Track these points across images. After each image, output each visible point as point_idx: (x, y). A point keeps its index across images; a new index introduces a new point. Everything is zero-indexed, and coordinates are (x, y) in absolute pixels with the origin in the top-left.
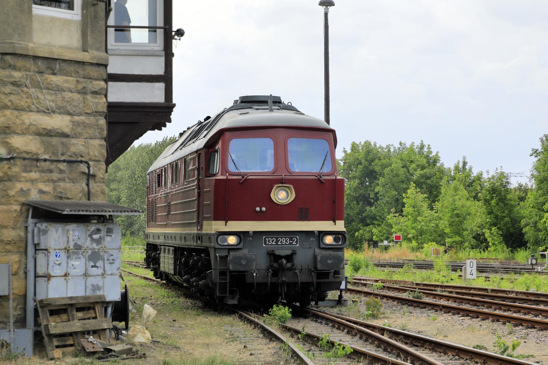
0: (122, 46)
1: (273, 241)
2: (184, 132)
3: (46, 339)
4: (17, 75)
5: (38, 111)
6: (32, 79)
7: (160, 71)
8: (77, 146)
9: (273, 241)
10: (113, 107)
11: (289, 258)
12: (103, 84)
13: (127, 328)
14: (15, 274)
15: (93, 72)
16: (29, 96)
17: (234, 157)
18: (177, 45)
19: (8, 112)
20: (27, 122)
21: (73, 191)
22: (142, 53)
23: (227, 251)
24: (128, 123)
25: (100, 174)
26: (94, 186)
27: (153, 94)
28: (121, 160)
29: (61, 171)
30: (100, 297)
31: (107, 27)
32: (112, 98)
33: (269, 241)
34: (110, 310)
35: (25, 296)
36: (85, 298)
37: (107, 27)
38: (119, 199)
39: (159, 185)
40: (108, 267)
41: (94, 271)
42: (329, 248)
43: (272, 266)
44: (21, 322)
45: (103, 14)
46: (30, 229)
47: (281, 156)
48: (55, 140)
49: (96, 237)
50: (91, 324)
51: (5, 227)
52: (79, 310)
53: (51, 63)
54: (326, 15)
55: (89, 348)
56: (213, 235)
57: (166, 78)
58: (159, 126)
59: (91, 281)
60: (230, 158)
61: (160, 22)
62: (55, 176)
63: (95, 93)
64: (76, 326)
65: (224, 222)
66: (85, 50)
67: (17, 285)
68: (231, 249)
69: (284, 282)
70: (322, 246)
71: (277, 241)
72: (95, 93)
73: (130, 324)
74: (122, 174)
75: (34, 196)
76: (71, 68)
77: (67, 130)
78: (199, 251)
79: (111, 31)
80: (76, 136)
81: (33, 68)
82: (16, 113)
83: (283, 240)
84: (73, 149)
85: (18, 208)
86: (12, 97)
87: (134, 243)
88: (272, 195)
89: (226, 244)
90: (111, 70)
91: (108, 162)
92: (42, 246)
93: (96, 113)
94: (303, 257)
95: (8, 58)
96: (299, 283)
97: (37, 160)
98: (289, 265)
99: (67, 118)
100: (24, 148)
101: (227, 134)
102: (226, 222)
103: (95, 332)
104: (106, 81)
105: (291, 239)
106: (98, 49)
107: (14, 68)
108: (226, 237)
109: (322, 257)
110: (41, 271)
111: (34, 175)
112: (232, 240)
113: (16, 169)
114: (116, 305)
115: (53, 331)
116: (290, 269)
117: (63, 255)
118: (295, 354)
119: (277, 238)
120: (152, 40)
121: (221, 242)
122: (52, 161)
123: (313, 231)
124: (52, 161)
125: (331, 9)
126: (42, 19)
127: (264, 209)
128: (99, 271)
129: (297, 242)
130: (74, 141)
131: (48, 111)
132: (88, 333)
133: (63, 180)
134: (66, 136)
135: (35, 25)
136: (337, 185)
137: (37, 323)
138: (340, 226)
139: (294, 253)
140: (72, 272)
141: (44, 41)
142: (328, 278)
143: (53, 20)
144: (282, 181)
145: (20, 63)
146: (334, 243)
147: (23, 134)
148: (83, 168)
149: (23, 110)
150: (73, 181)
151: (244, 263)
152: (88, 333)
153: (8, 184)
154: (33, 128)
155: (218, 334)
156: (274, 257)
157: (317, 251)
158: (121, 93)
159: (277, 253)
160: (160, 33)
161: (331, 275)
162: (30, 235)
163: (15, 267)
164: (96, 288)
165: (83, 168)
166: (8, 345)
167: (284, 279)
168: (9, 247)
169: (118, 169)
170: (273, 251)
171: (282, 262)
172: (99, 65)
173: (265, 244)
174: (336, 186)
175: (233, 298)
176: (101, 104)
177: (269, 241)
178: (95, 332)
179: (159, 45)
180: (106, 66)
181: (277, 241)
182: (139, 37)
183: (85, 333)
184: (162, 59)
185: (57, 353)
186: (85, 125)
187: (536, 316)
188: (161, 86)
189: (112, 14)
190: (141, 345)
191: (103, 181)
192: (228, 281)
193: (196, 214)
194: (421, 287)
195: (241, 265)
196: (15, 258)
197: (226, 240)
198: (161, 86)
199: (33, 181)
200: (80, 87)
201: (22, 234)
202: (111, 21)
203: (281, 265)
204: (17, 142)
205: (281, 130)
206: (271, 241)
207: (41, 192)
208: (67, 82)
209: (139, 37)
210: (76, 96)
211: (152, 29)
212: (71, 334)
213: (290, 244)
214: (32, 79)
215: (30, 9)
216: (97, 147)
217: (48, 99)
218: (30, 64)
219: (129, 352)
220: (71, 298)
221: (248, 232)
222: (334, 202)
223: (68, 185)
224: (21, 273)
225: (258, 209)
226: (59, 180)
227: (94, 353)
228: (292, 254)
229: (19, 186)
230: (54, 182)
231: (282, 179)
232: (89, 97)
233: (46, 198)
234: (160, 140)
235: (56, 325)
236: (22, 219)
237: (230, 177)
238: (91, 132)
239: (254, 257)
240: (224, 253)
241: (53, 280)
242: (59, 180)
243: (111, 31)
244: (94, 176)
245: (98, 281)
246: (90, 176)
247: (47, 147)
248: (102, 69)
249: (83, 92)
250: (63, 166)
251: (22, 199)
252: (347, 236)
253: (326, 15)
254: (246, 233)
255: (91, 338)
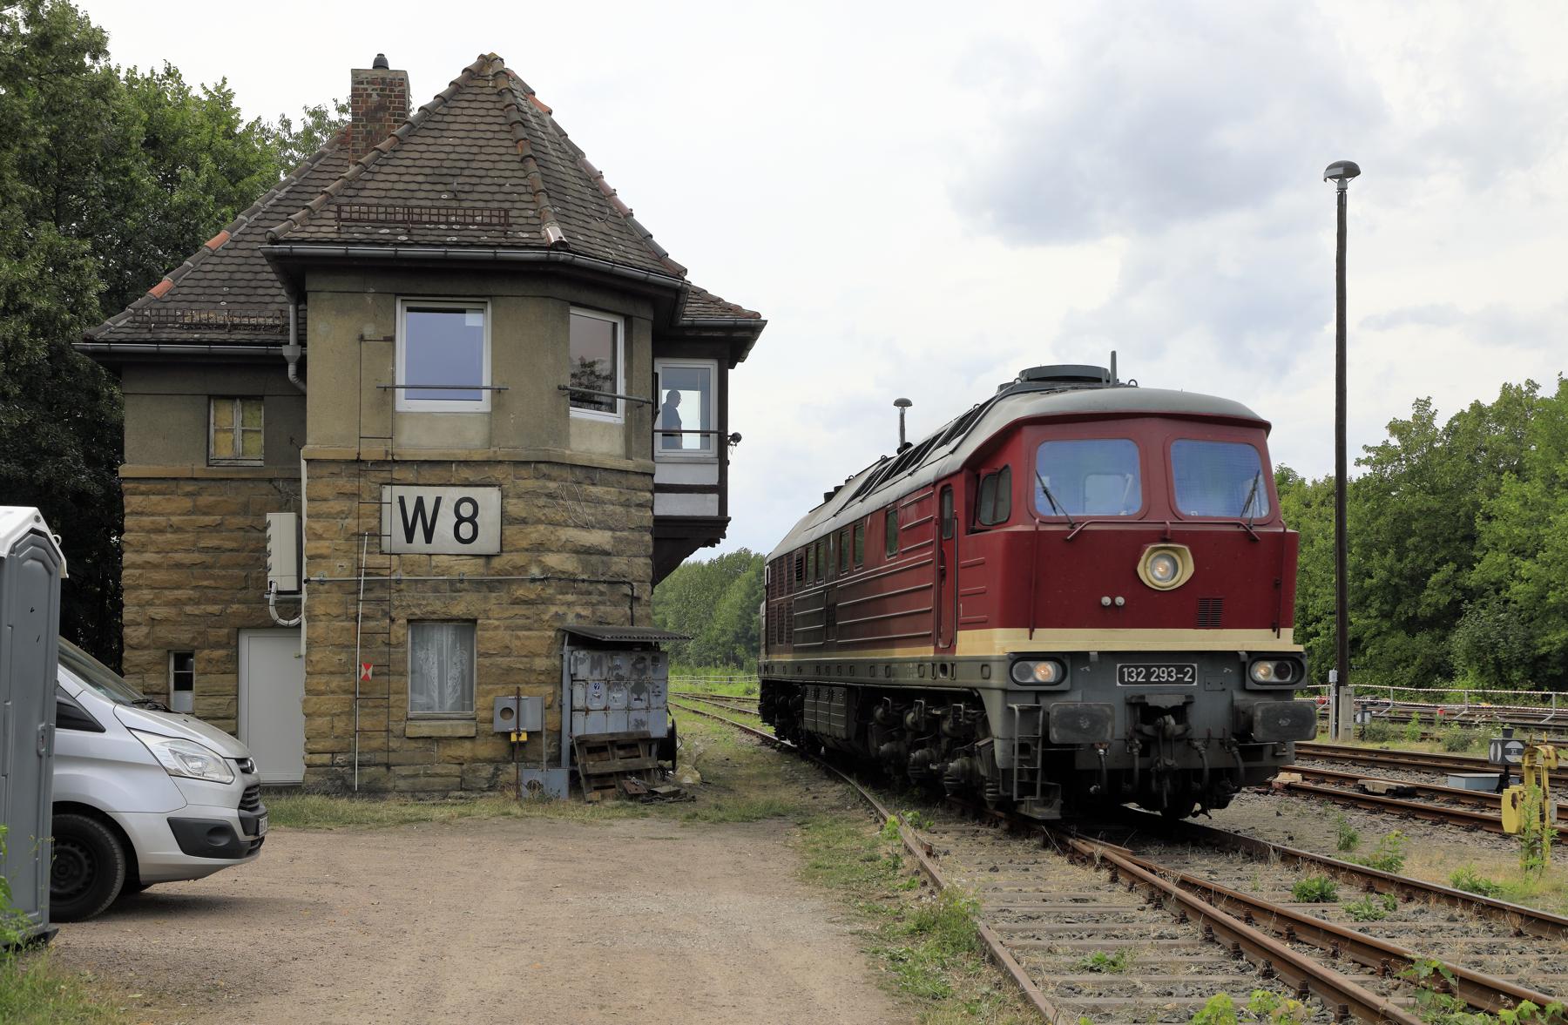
0: (672, 453)
1: (1138, 674)
2: (838, 489)
3: (583, 781)
4: (552, 485)
5: (576, 526)
6: (568, 491)
7: (714, 481)
8: (619, 564)
9: (1138, 674)
10: (660, 521)
11: (1180, 712)
12: (648, 495)
13: (674, 769)
14: (549, 707)
15: (638, 482)
16: (566, 509)
17: (1046, 480)
18: (734, 453)
19: (541, 527)
20: (563, 538)
21: (614, 618)
22: (692, 461)
23: (1032, 697)
24: (678, 537)
25: (645, 597)
26: (639, 611)
27: (704, 506)
28: (667, 581)
29: (601, 594)
30: (644, 733)
31: (654, 431)
32: (659, 511)
33: (1130, 675)
34: (654, 749)
35: (560, 732)
36: (628, 734)
37: (654, 431)
38: (665, 624)
39: (799, 578)
40: (653, 700)
41: (638, 704)
42: (1264, 691)
43: (1140, 732)
44: (555, 761)
45: (649, 417)
46: (566, 657)
47: (1157, 481)
48: (594, 559)
49: (640, 666)
50: (634, 764)
51: (539, 655)
52: (621, 747)
53: (590, 472)
54: (902, 416)
55: (632, 790)
56: (1000, 660)
57: (721, 489)
58: (712, 542)
59: (634, 715)
60: (1038, 484)
61: (714, 426)
62: (595, 598)
63: (640, 505)
64: (617, 765)
65: (1026, 631)
66: (628, 458)
67: (552, 718)
68: (1043, 691)
69: (1169, 770)
70: (1250, 685)
71: (1148, 675)
72: (640, 505)
73: (678, 762)
74: (671, 596)
75: (571, 621)
76: (613, 478)
77: (608, 547)
78: (938, 697)
79: (658, 436)
80: (618, 554)
81: (570, 478)
82: (551, 528)
83: (1163, 673)
84: (614, 568)
85: (552, 634)
86: (546, 511)
87: (682, 672)
88: (1140, 569)
89: (1031, 680)
90: (658, 479)
91: (654, 583)
92: (580, 677)
93: (641, 528)
94: (1210, 710)
95: (542, 466)
96: (1207, 773)
97: (575, 581)
98: (1179, 729)
99: (609, 533)
100: (560, 568)
101: (1028, 431)
102: (1032, 631)
103: (638, 773)
104: (652, 493)
105: (1180, 670)
106: (644, 457)
107: (549, 478)
108: (1031, 664)
109: (1267, 711)
110: (578, 704)
111: (570, 598)
112: (1044, 672)
113: (550, 591)
114: (660, 741)
115: (591, 771)
116: (1179, 738)
117: (603, 686)
118: (1349, 1003)
119: (1148, 668)
120: (705, 445)
121: (1019, 674)
122: (591, 582)
123: (1236, 653)
124: (591, 582)
125: (908, 409)
126: (580, 421)
127: (1120, 600)
128: (643, 705)
129: (1193, 677)
130: (615, 559)
131: (587, 526)
132: (631, 773)
133: (603, 603)
134: (607, 554)
135: (573, 430)
136: (1282, 548)
137: (573, 762)
138: (1285, 641)
139: (1189, 702)
140: (613, 705)
141: (583, 448)
142: (1261, 759)
143: (593, 423)
144: (1164, 537)
145: (555, 472)
146: (1275, 680)
147: (558, 551)
148: (626, 589)
149: (558, 524)
150: (615, 604)
151: (1085, 725)
152: (631, 773)
153: (542, 607)
154: (569, 545)
155: (777, 775)
156: (1144, 712)
157: (1239, 697)
158: (668, 506)
159: (1153, 701)
160: (714, 438)
161: (1268, 751)
162: (566, 665)
163: (550, 699)
164: (640, 723)
165: (626, 589)
166: (541, 786)
167: (1169, 762)
168: (542, 678)
169: (665, 591)
170: (1143, 697)
171: (1166, 723)
172: (644, 474)
173: (1122, 681)
174: (1282, 548)
175: (1047, 803)
176: (646, 517)
177: (1130, 675)
178: (638, 773)
179: (713, 452)
180: (652, 475)
181: (1148, 675)
182: (691, 442)
183: (624, 774)
184: (717, 467)
185: (596, 795)
186: (628, 541)
187: (1317, 783)
188: (715, 497)
189: (660, 416)
190: (690, 786)
191: (648, 603)
192: (1039, 766)
193: (931, 619)
194: (1319, 766)
195: (1079, 730)
196: (549, 689)
197: (1030, 672)
198: (715, 497)
199: (569, 604)
200: (623, 499)
201: (557, 663)
202: (659, 425)
203: (1162, 729)
204: (552, 560)
205: (1156, 421)
206: (1135, 675)
207: (579, 616)
208: (608, 493)
209: (691, 442)
210: (619, 509)
211: (705, 433)
212: (610, 775)
213: (1179, 680)
214: (568, 491)
215: (567, 412)
216: (641, 566)
217: (587, 512)
218: (566, 473)
219: (675, 794)
220: (612, 734)
221: (1086, 654)
222: (1277, 585)
223: (609, 609)
224: (556, 706)
225: (1106, 600)
226: (600, 603)
227: (637, 796)
228: (1185, 704)
229: (553, 609)
230: (593, 605)
231: (1165, 532)
232: (633, 510)
233: (584, 624)
234: (716, 557)
235: (594, 766)
236: (557, 646)
237: (1042, 528)
238: (634, 549)
239: (1108, 710)
240: (1029, 703)
241: (592, 714)
242: (600, 603)
243: (658, 436)
244: (638, 599)
245: (642, 716)
246: (634, 599)
247: (585, 566)
248: (648, 478)
249: (627, 505)
250: (602, 587)
251: (557, 625)
252: (1307, 662)
253: (902, 416)
254: (1080, 657)
255: (633, 779)
